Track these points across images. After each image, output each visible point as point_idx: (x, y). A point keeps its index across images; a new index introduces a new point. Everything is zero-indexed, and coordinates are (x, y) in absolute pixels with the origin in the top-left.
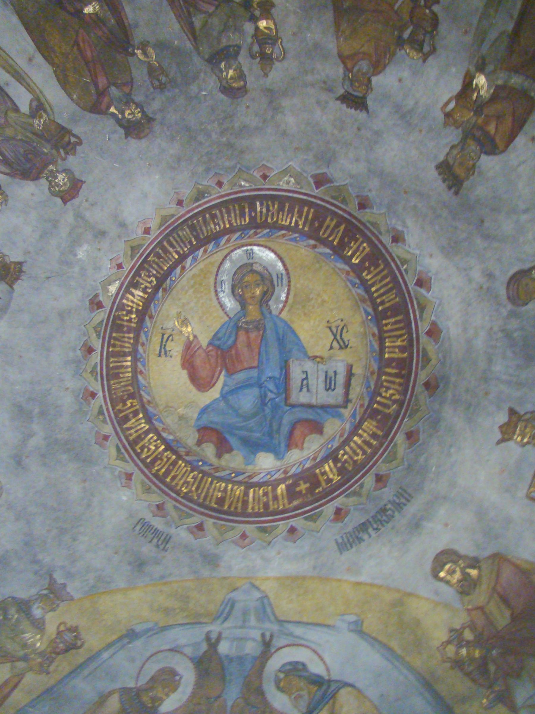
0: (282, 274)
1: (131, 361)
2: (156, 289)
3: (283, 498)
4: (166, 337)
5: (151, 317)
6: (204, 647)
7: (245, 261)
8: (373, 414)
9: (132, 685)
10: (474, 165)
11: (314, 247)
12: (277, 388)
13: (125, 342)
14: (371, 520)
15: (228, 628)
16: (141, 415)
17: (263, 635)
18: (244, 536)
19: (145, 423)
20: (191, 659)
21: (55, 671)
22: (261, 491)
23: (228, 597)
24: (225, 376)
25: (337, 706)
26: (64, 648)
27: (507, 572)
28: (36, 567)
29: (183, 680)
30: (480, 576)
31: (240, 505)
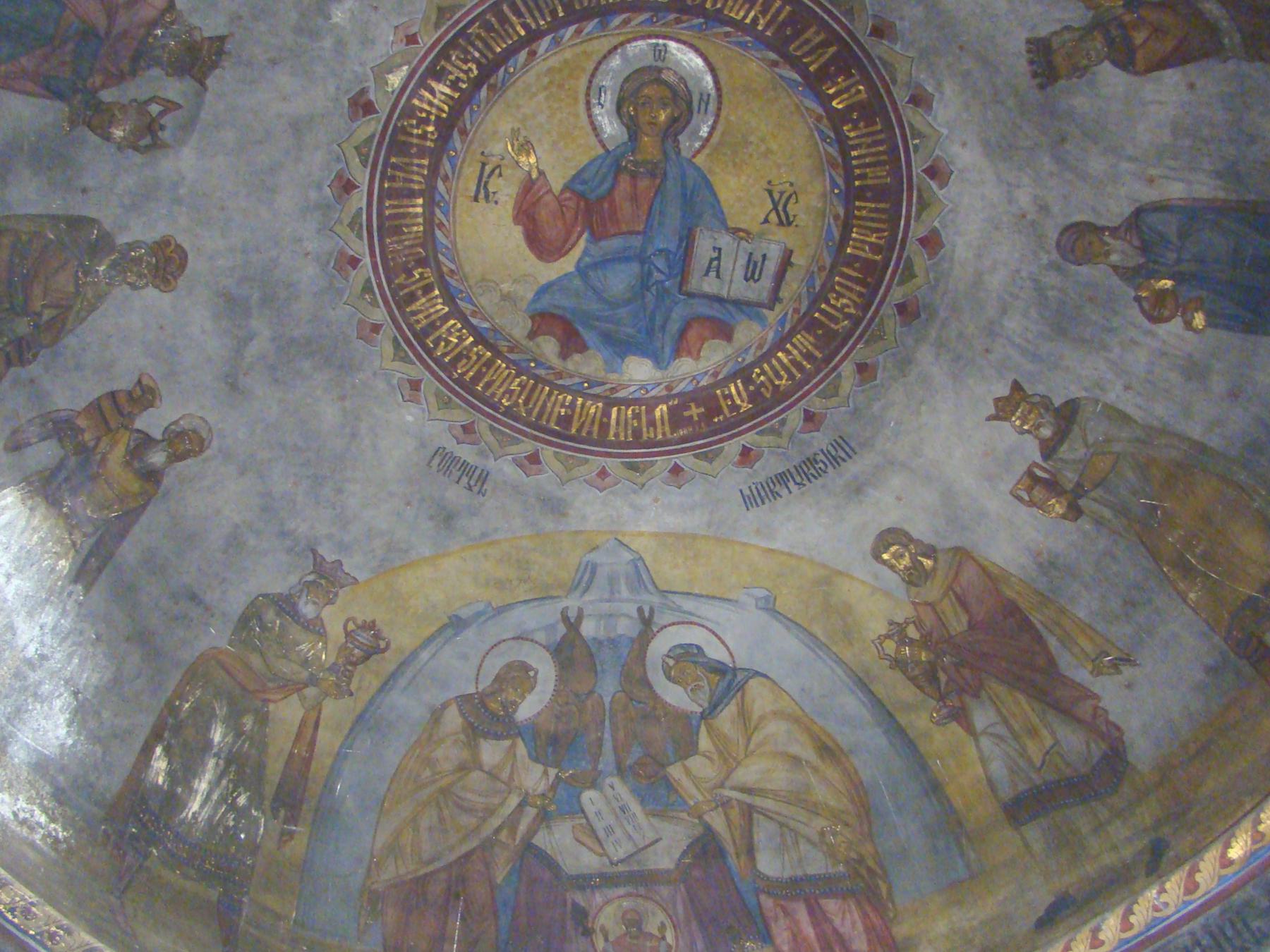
0: (709, 95)
1: (423, 206)
2: (477, 84)
3: (663, 423)
4: (488, 169)
5: (464, 133)
6: (562, 629)
7: (649, 61)
8: (809, 324)
9: (472, 690)
10: (1086, 68)
11: (774, 64)
12: (669, 267)
13: (413, 172)
14: (793, 470)
15: (592, 602)
16: (437, 292)
17: (640, 610)
18: (603, 473)
19: (443, 304)
20: (546, 648)
21: (359, 688)
22: (630, 412)
23: (585, 559)
24: (587, 241)
25: (748, 699)
26: (362, 654)
27: (969, 574)
28: (288, 543)
29: (539, 676)
30: (934, 569)
31: (596, 428)
